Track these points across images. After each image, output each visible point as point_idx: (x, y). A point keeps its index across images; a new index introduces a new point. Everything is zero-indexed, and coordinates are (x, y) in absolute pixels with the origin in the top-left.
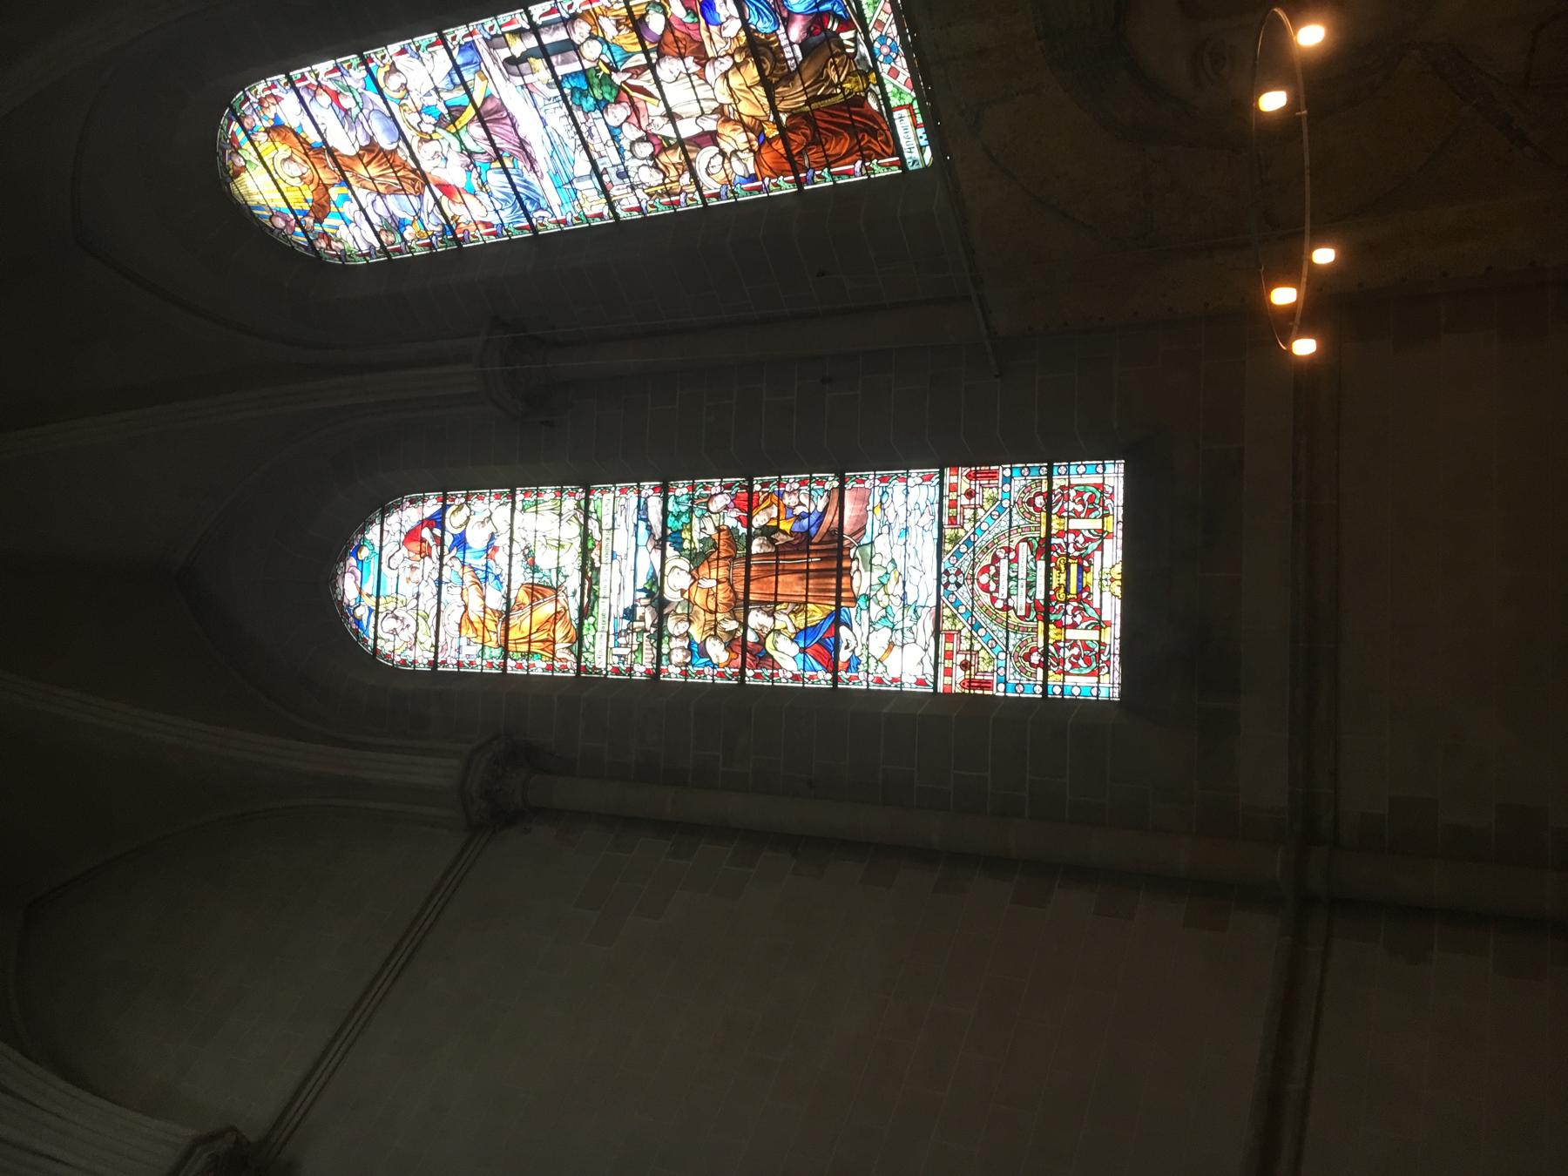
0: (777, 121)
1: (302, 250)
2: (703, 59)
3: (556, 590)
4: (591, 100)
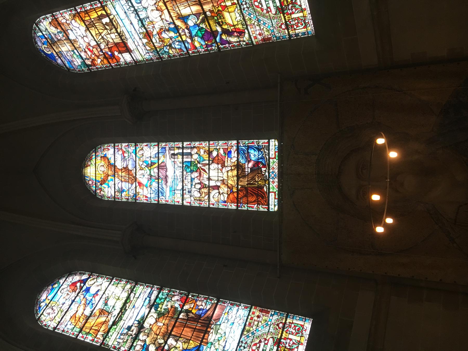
0: (237, 187)
1: (92, 192)
2: (223, 166)
3: (109, 313)
4: (190, 169)
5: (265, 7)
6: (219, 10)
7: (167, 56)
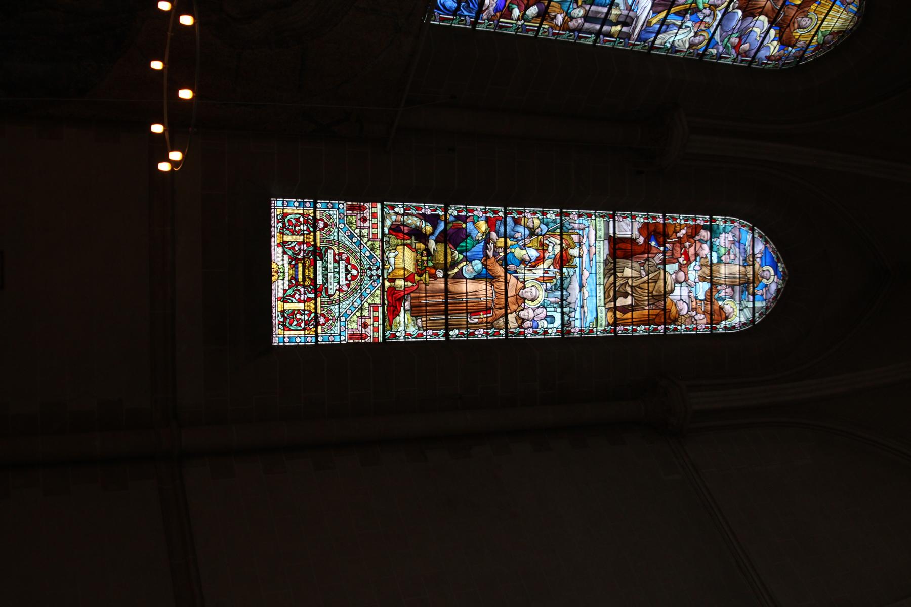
5: (342, 264)
6: (420, 275)
7: (548, 216)
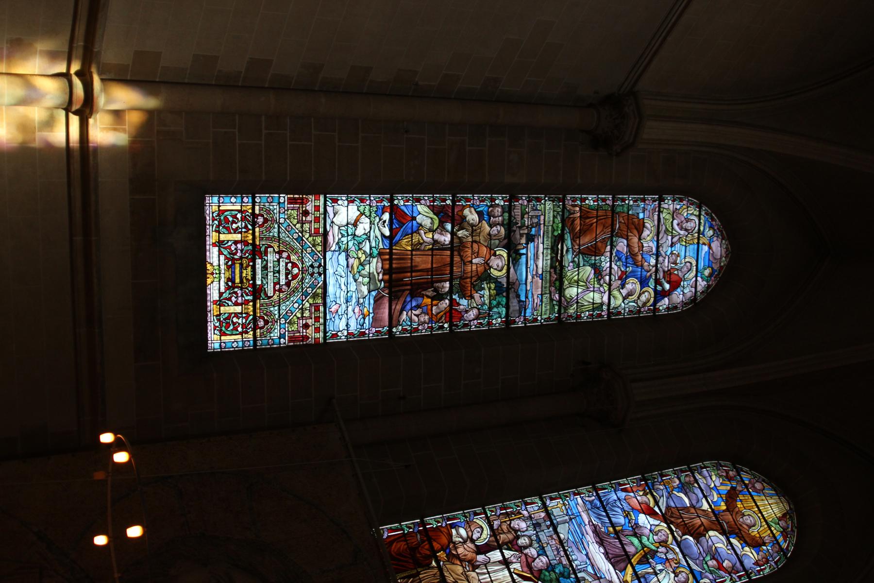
1: (745, 469)
